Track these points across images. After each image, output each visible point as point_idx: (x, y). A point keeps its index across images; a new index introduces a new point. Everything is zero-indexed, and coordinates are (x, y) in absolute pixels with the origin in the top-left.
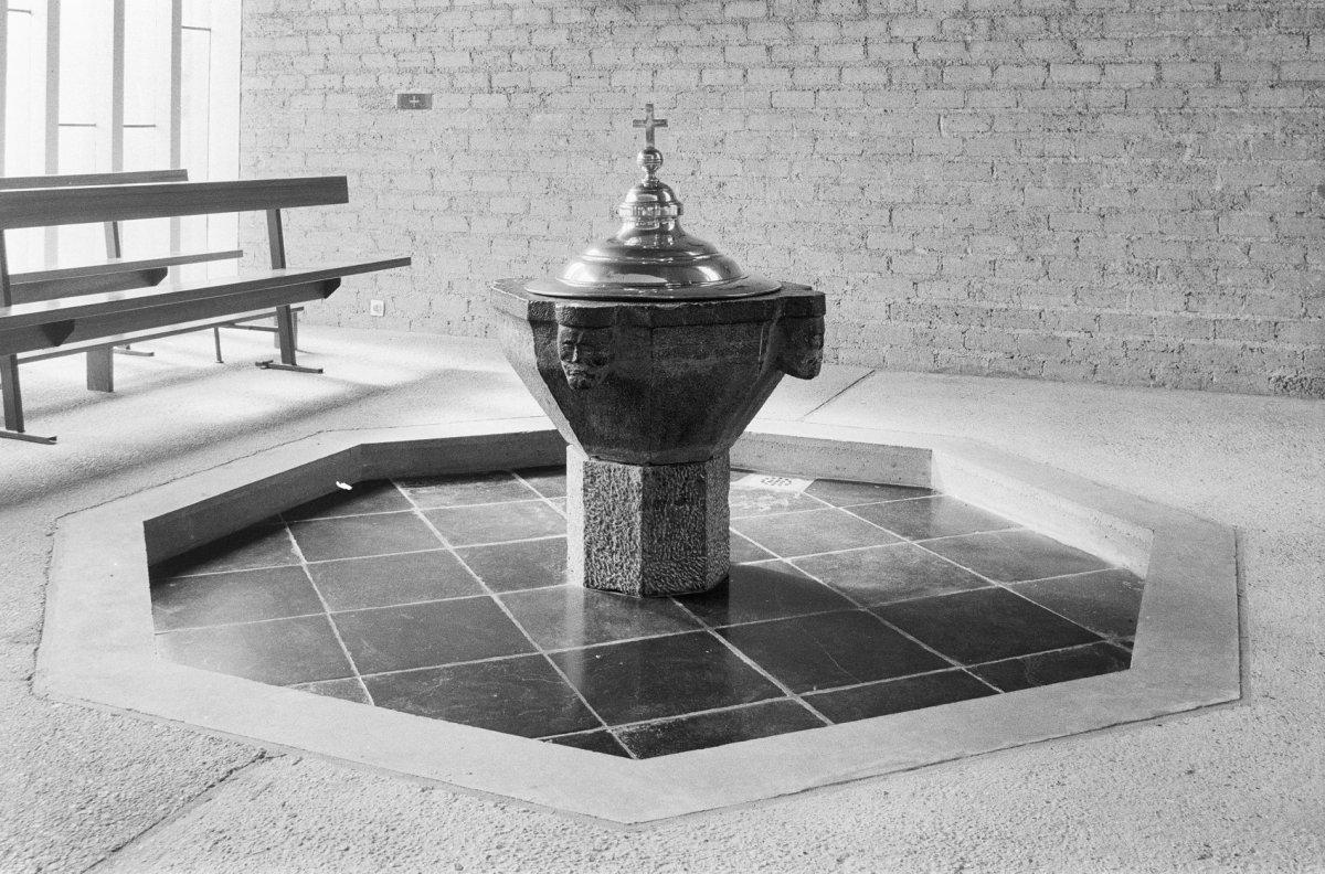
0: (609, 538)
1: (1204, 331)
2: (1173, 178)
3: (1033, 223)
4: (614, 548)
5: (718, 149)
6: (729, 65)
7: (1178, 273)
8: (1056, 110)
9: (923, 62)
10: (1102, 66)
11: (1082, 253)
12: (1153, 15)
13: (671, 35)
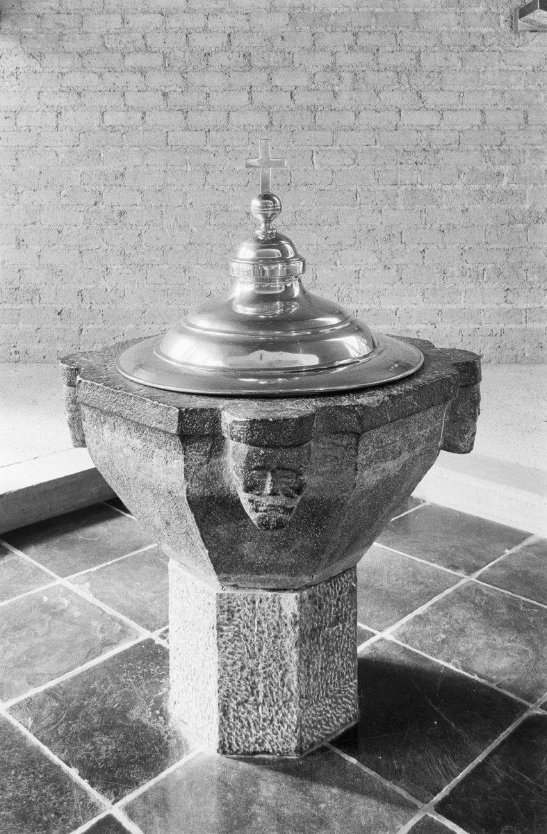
0: (254, 686)
1: (518, 317)
2: (495, 200)
3: (388, 239)
4: (260, 699)
5: (119, 181)
6: (128, 108)
7: (500, 273)
8: (405, 147)
9: (300, 108)
10: (441, 113)
11: (427, 262)
12: (479, 73)
13: (74, 80)
